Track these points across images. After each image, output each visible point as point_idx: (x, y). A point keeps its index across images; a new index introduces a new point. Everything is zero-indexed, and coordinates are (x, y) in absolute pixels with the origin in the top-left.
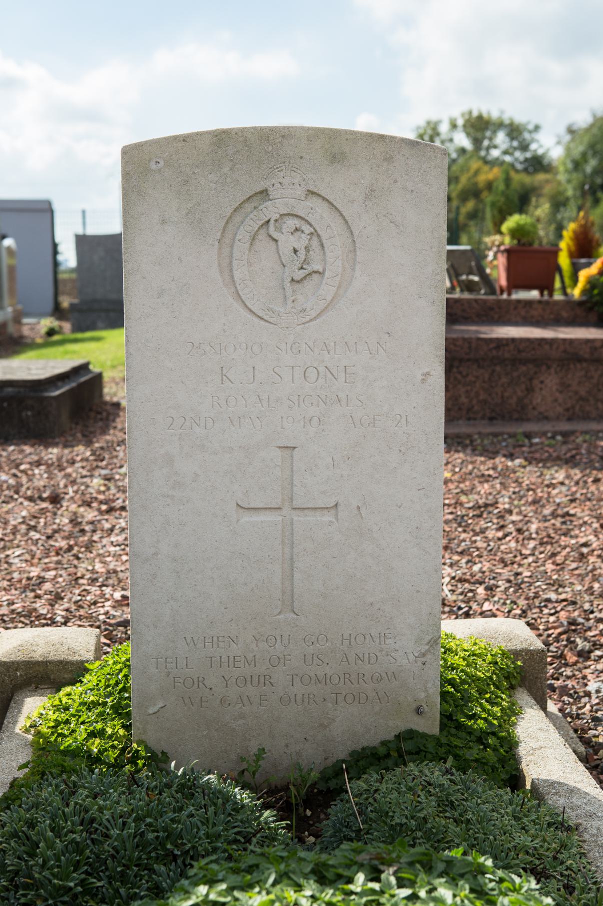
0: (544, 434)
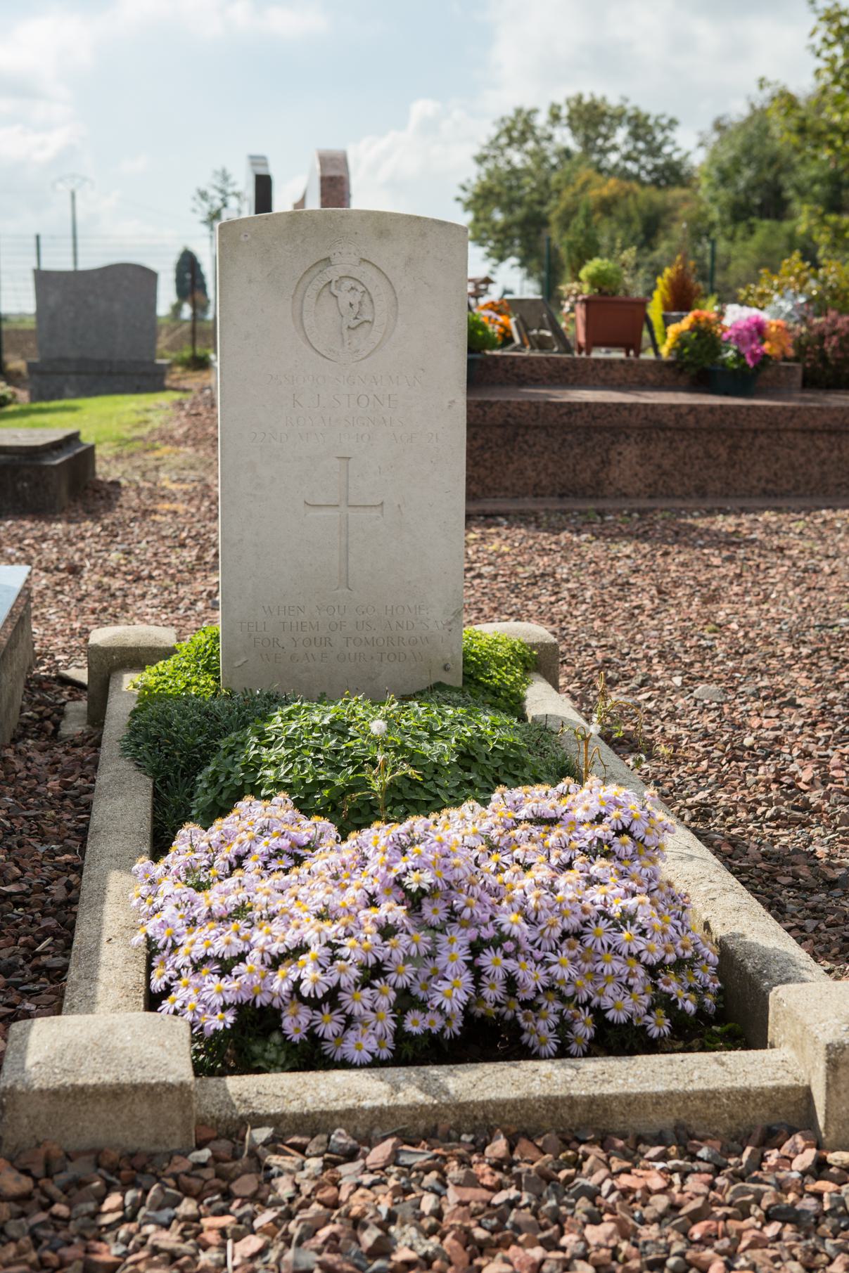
0: (620, 511)
